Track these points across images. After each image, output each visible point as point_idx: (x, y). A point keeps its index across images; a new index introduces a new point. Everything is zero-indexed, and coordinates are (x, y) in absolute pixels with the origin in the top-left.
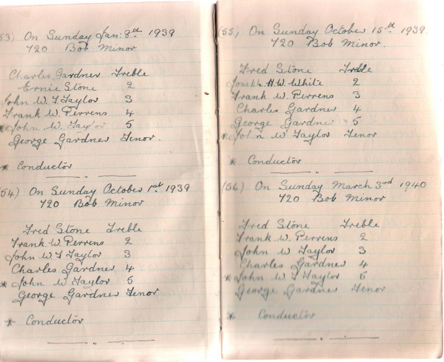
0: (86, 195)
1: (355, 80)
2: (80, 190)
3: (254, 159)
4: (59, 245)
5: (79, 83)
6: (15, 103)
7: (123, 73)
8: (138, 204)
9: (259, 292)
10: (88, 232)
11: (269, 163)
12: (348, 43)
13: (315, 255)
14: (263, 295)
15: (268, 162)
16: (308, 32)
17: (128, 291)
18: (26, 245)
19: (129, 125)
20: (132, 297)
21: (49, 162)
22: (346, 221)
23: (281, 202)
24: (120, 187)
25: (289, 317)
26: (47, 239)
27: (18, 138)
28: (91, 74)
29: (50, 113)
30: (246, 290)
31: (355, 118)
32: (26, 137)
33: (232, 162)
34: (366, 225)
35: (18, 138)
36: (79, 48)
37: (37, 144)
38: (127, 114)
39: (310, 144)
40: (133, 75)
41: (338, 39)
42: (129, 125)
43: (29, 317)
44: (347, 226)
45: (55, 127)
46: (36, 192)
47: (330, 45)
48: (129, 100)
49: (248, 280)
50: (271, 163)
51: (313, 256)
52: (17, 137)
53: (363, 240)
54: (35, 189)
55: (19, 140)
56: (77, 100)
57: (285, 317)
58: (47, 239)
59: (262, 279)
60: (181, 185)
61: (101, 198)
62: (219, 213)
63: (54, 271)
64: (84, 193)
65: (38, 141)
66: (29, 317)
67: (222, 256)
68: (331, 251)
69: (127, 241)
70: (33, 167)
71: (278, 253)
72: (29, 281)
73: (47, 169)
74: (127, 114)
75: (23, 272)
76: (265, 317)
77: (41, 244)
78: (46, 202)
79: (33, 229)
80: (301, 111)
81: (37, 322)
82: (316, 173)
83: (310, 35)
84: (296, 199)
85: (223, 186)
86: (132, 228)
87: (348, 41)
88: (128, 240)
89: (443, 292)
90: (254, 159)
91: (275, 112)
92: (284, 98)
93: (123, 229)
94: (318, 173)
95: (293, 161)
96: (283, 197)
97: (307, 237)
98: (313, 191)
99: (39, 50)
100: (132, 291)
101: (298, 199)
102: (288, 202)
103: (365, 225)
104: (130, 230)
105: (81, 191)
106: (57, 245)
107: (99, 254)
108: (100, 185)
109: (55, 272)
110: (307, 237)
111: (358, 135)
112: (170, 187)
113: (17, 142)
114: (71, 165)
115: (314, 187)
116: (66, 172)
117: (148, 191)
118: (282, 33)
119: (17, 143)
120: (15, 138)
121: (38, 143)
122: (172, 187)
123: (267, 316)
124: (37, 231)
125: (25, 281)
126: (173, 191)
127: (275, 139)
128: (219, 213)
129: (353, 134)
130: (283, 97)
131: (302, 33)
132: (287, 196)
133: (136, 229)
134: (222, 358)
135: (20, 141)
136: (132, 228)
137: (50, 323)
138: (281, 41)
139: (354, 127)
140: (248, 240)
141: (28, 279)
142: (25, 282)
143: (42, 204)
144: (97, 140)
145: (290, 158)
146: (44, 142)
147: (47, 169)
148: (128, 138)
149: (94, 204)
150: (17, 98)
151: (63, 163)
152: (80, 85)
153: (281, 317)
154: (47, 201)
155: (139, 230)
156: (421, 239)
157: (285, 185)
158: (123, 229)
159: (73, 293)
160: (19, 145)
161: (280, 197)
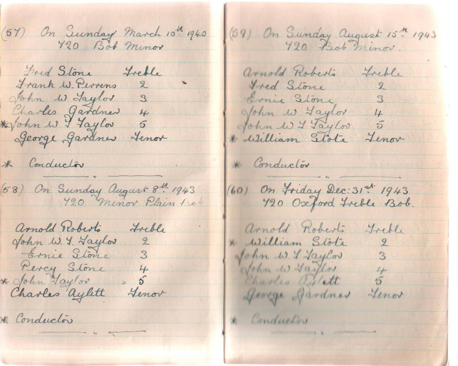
0: (311, 195)
1: (142, 82)
2: (87, 188)
3: (260, 161)
4: (59, 244)
5: (304, 82)
8: (132, 204)
9: (268, 296)
11: (278, 167)
13: (319, 261)
14: (271, 300)
15: (277, 165)
16: (322, 36)
19: (143, 125)
20: (137, 298)
22: (370, 226)
25: (283, 322)
27: (72, 136)
29: (288, 112)
30: (256, 294)
31: (142, 122)
32: (33, 132)
33: (236, 165)
34: (82, 229)
35: (72, 136)
36: (108, 46)
37: (45, 142)
39: (22, 145)
44: (137, 230)
45: (287, 127)
46: (42, 190)
48: (144, 99)
50: (52, 166)
51: (318, 261)
52: (70, 134)
54: (266, 187)
56: (92, 98)
57: (279, 322)
60: (194, 188)
62: (225, 217)
64: (91, 192)
65: (45, 137)
69: (144, 242)
71: (275, 258)
72: (29, 279)
79: (375, 228)
81: (26, 320)
82: (326, 177)
84: (280, 203)
85: (228, 190)
86: (156, 227)
87: (131, 44)
88: (385, 241)
90: (260, 161)
94: (328, 177)
95: (76, 166)
96: (267, 202)
98: (92, 196)
99: (298, 49)
101: (282, 203)
103: (154, 230)
104: (154, 230)
105: (87, 190)
111: (380, 139)
112: (386, 189)
113: (25, 139)
115: (309, 192)
117: (173, 191)
119: (24, 141)
120: (68, 135)
121: (45, 141)
122: (388, 189)
123: (261, 321)
125: (25, 280)
126: (389, 193)
127: (248, 142)
128: (225, 217)
129: (375, 138)
131: (316, 36)
132: (271, 202)
134: (225, 362)
136: (156, 227)
137: (39, 322)
139: (141, 129)
141: (28, 277)
142: (26, 280)
143: (66, 202)
144: (105, 139)
146: (53, 140)
148: (137, 137)
149: (408, 204)
152: (305, 84)
153: (275, 321)
154: (70, 199)
156: (427, 245)
157: (62, 188)
159: (91, 292)
160: (26, 143)
161: (264, 202)
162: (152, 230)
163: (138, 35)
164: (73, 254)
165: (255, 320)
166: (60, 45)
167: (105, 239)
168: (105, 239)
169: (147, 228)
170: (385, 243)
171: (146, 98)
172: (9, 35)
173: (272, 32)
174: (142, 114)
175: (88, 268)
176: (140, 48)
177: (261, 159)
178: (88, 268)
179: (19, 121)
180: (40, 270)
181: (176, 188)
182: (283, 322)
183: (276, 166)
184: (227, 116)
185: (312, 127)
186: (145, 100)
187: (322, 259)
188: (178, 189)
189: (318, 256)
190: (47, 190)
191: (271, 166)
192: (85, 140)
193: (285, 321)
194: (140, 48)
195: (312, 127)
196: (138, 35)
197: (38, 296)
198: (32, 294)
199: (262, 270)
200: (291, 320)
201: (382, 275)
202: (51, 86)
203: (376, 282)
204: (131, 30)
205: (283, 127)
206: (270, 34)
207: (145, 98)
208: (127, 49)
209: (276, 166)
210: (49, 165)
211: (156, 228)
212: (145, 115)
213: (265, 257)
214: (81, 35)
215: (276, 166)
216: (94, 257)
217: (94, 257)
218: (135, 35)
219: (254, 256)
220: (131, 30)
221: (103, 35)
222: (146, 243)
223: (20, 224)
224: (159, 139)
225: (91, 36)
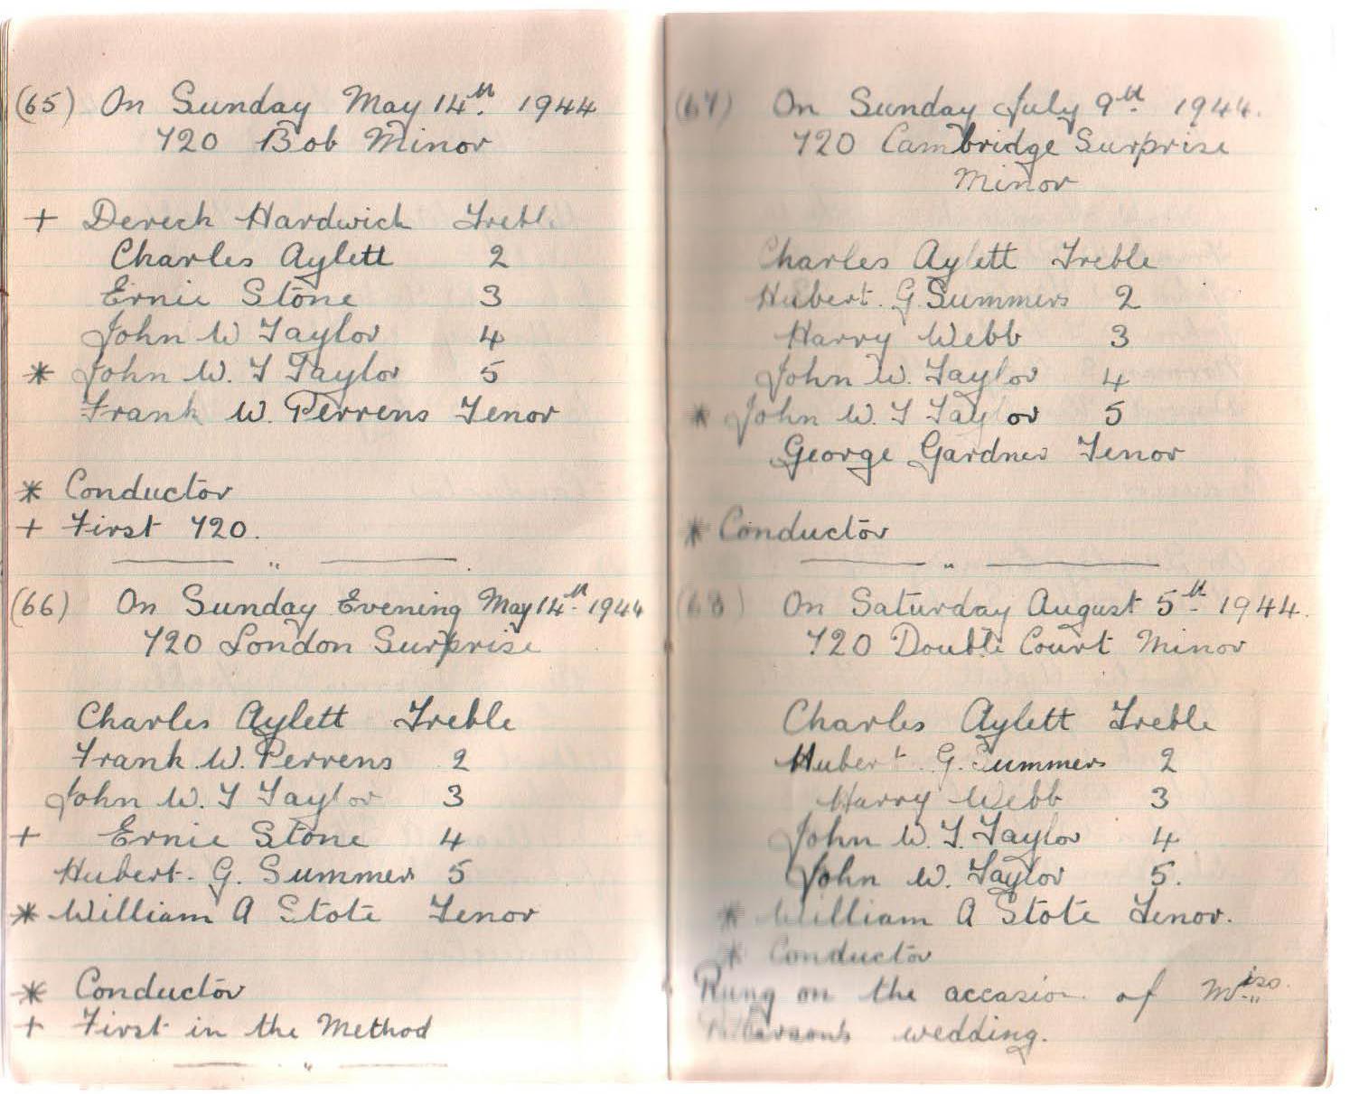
7: (133, 298)
10: (509, 726)
18: (123, 763)
20: (1150, 926)
21: (816, 520)
24: (1133, 596)
26: (195, 747)
28: (832, 298)
38: (1104, 383)
40: (1114, 266)
42: (1114, 415)
49: (836, 882)
53: (1166, 771)
55: (802, 449)
58: (195, 747)
61: (1016, 631)
74: (1104, 383)
77: (174, 760)
78: (829, 633)
80: (138, 421)
86: (1182, 717)
89: (1330, 931)
91: (183, 418)
92: (220, 379)
93: (453, 719)
97: (290, 758)
100: (1149, 903)
102: (834, 655)
103: (995, 337)
106: (230, 768)
108: (1014, 592)
110: (290, 758)
114: (885, 529)
116: (870, 547)
124: (441, 723)
130: (219, 374)
133: (497, 721)
135: (805, 455)
140: (108, 763)
155: (1205, 726)
158: (453, 719)
162: (470, 722)
163: (387, 110)
164: (376, 642)
166: (162, 140)
167: (176, 715)
168: (176, 715)
170: (499, 256)
171: (499, 295)
172: (1111, 421)
174: (487, 342)
176: (414, 145)
180: (476, 651)
181: (597, 601)
185: (265, 337)
186: (496, 301)
188: (603, 604)
194: (414, 145)
195: (265, 337)
196: (387, 110)
198: (157, 763)
204: (363, 95)
207: (495, 295)
208: (369, 149)
212: (495, 345)
214: (213, 111)
218: (379, 108)
220: (363, 95)
221: (279, 108)
222: (461, 766)
224: (539, 418)
225: (242, 111)
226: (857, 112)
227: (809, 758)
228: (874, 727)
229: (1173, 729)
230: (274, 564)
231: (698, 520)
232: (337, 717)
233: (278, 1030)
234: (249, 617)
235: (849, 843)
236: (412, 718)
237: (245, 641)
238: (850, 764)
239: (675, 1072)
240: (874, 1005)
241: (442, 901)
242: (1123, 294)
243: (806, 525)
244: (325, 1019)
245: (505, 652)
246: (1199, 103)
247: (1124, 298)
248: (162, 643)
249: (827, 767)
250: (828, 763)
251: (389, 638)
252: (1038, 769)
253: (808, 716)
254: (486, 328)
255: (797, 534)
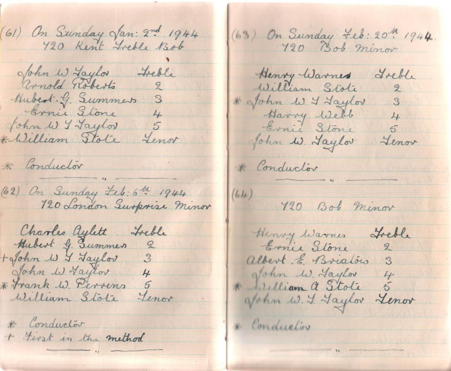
6: (36, 74)
11: (282, 170)
12: (360, 48)
17: (83, 111)
23: (284, 210)
25: (285, 328)
33: (242, 167)
41: (351, 43)
43: (76, 228)
46: (36, 192)
47: (343, 49)
57: (281, 328)
59: (279, 302)
63: (113, 87)
66: (76, 228)
67: (228, 265)
68: (353, 274)
70: (402, 142)
73: (60, 168)
75: (39, 288)
76: (260, 326)
83: (324, 40)
86: (156, 231)
104: (154, 233)
107: (115, 258)
109: (113, 89)
118: (299, 37)
123: (261, 326)
128: (227, 221)
138: (291, 46)
145: (306, 164)
147: (60, 168)
150: (39, 67)
151: (306, 164)
165: (256, 326)
169: (147, 232)
173: (276, 34)
175: (99, 205)
177: (264, 162)
178: (99, 205)
179: (18, 121)
182: (285, 328)
183: (281, 169)
184: (229, 119)
187: (343, 304)
189: (339, 301)
190: (65, 140)
191: (274, 169)
192: (42, 115)
193: (288, 327)
197: (104, 88)
199: (270, 300)
200: (294, 327)
201: (389, 281)
202: (46, 287)
203: (384, 288)
205: (294, 142)
206: (274, 35)
209: (281, 169)
210: (47, 167)
211: (157, 231)
213: (278, 302)
215: (281, 169)
216: (101, 207)
217: (101, 207)
219: (265, 300)
223: (34, 187)
226: (58, 35)
227: (24, 243)
228: (384, 236)
229: (395, 237)
230: (104, 179)
231: (243, 164)
232: (103, 232)
233: (91, 339)
234: (74, 196)
235: (277, 276)
236: (376, 234)
237: (73, 204)
238: (38, 245)
239: (229, 366)
240: (63, 342)
241: (382, 296)
242: (158, 85)
243: (289, 165)
244: (109, 337)
245: (156, 208)
246: (413, 35)
247: (157, 86)
248: (47, 205)
249: (29, 246)
250: (28, 99)
251: (120, 204)
252: (102, 248)
253: (29, 229)
254: (394, 113)
255: (285, 169)
